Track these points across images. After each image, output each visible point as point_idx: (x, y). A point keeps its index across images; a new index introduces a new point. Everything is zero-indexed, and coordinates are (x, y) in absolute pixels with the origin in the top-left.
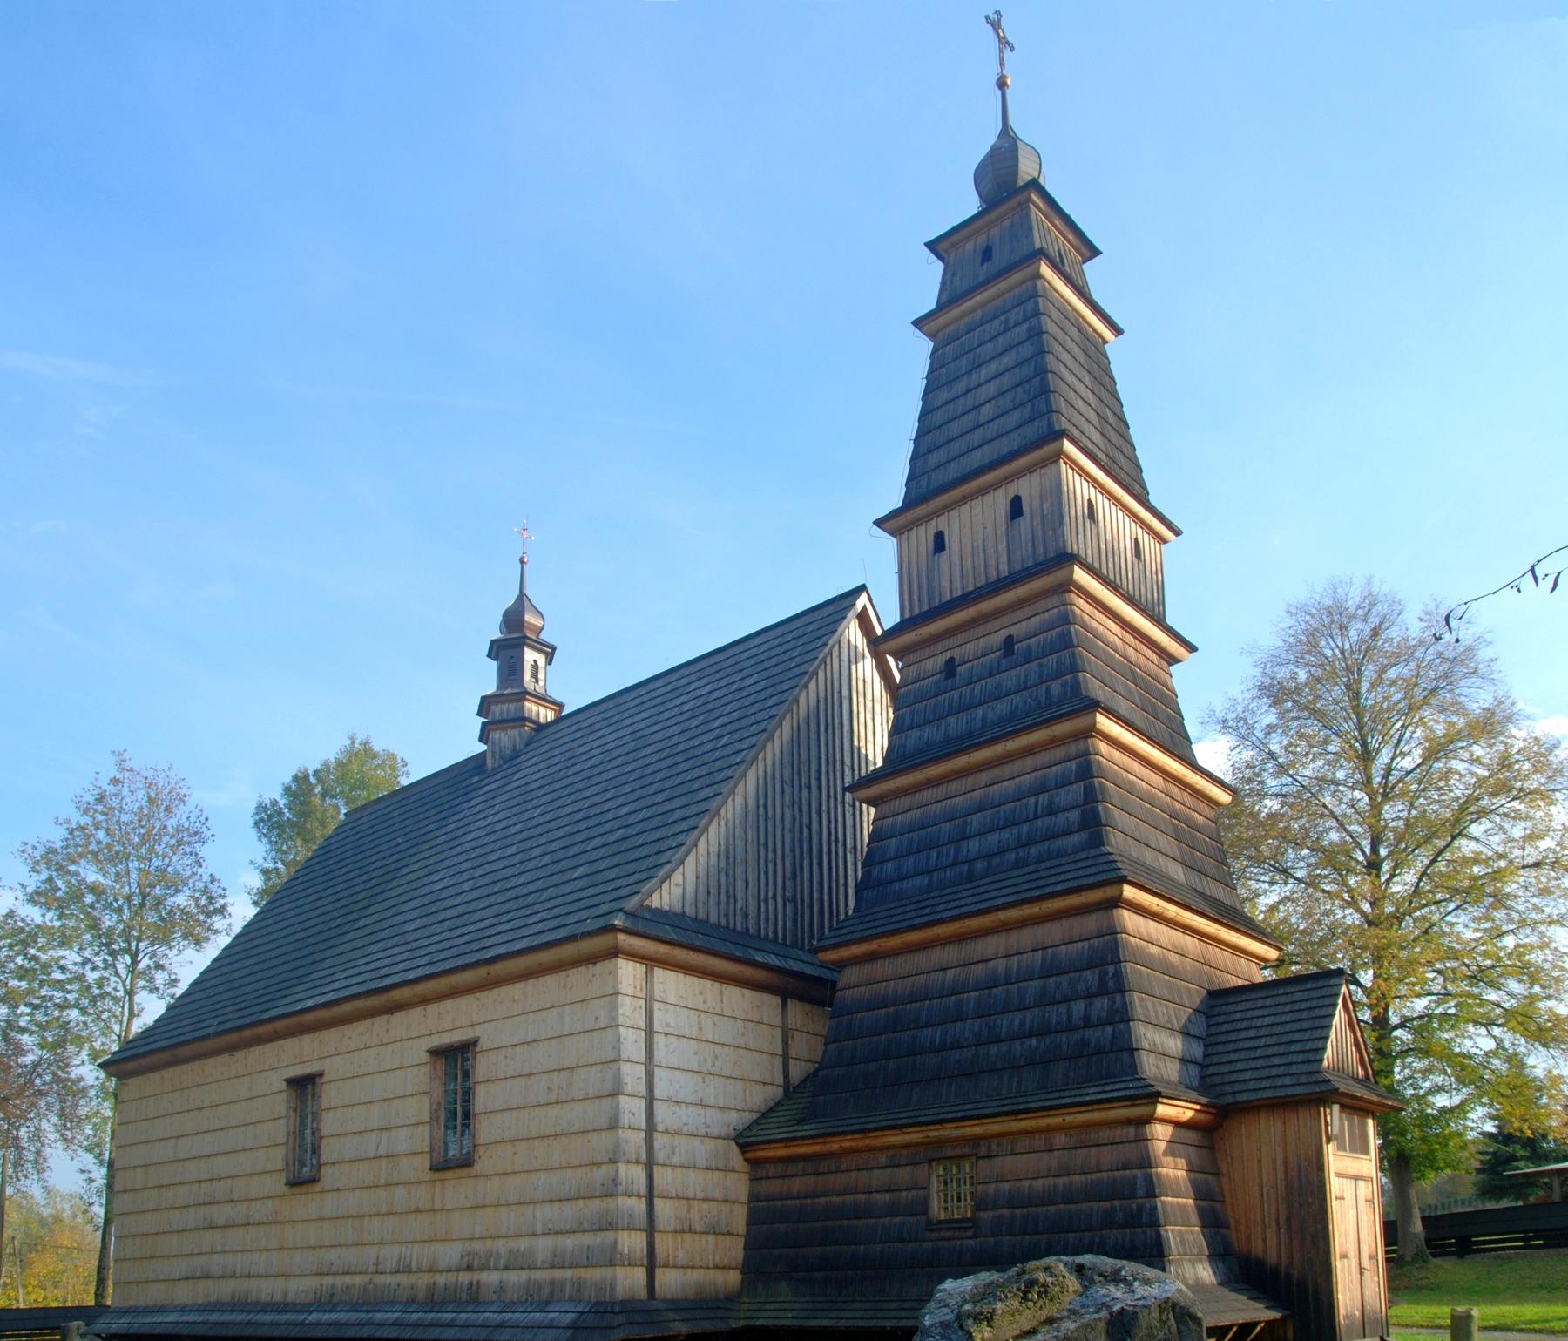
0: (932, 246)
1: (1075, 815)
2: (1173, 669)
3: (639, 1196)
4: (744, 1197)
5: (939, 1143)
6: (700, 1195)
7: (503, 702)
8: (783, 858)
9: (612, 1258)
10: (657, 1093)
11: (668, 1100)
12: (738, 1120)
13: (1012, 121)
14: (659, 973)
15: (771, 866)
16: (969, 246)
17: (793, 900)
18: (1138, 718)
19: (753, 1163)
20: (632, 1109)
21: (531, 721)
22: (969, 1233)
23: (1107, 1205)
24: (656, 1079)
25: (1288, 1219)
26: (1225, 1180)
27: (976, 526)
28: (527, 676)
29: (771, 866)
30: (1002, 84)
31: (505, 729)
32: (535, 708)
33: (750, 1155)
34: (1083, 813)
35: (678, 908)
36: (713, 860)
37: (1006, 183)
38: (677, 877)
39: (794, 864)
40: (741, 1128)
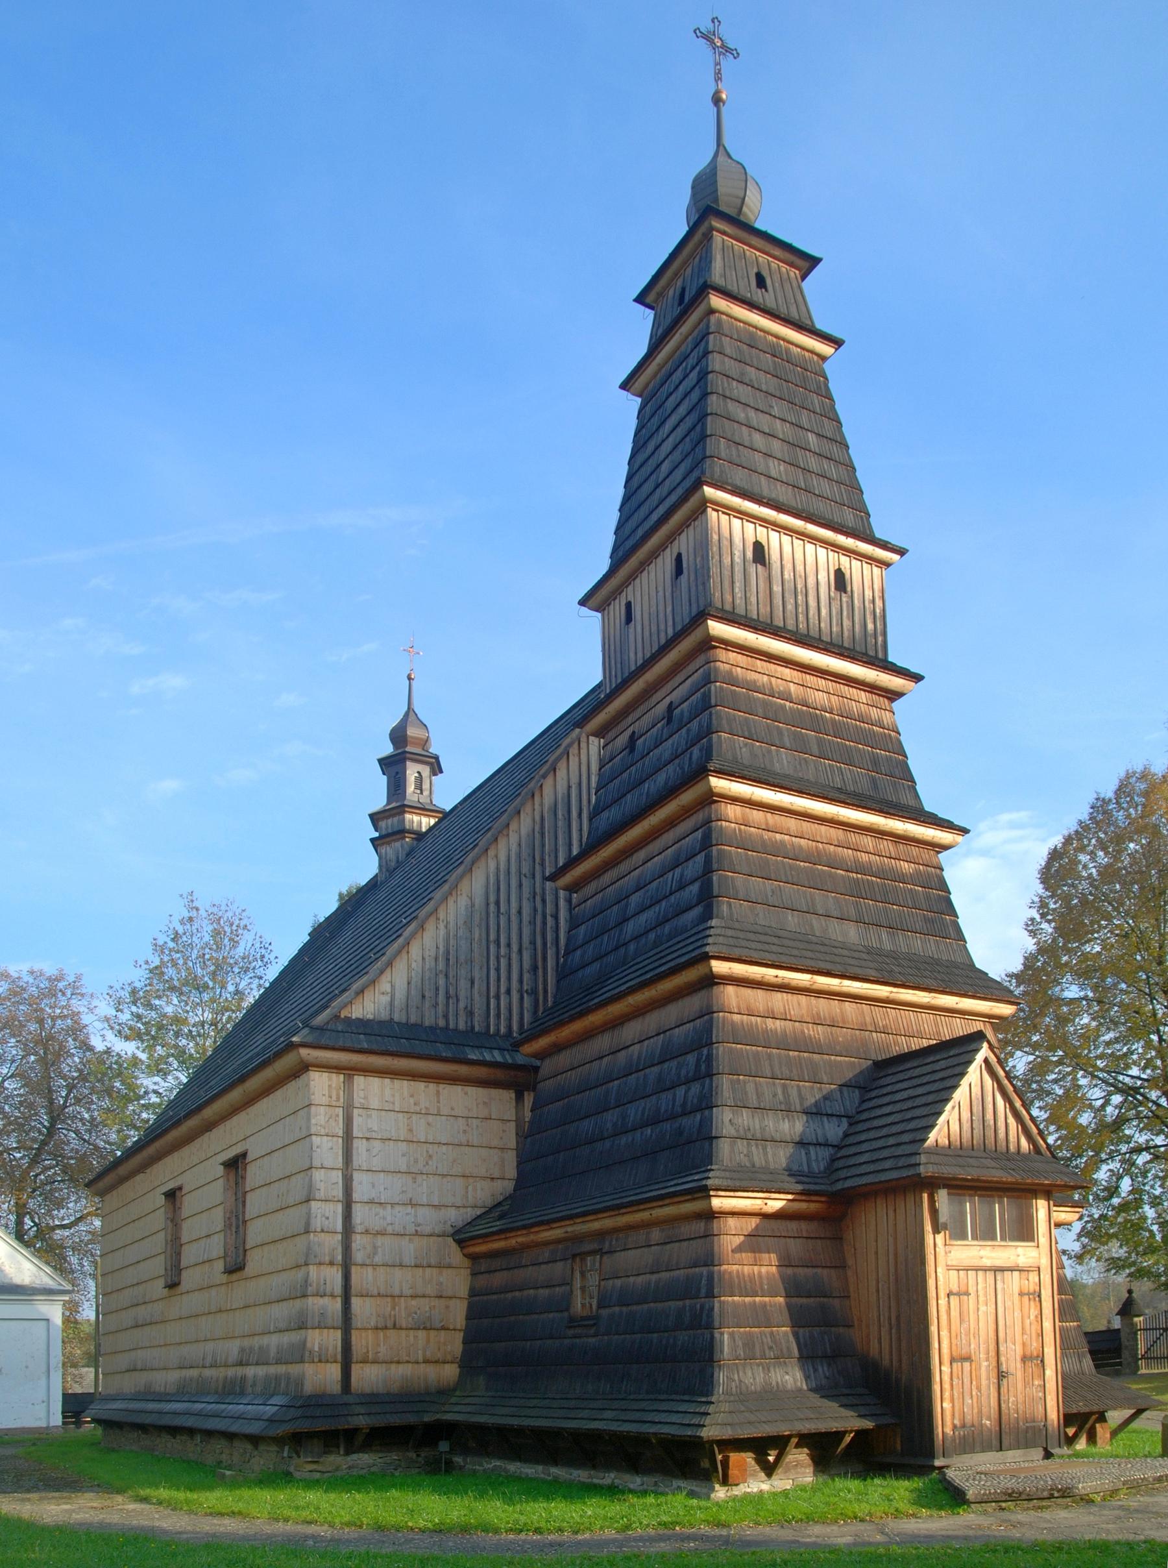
0: (640, 299)
2: (896, 705)
3: (333, 1296)
4: (464, 1291)
5: (578, 1239)
6: (408, 1292)
7: (388, 818)
8: (520, 951)
9: (299, 1354)
10: (356, 1196)
11: (371, 1202)
12: (456, 1217)
13: (727, 142)
14: (359, 1081)
15: (503, 962)
16: (671, 292)
17: (534, 992)
19: (474, 1258)
20: (328, 1214)
21: (410, 832)
22: (592, 1331)
23: (681, 1303)
24: (355, 1183)
26: (849, 1273)
27: (651, 589)
28: (411, 788)
29: (503, 962)
30: (717, 100)
31: (389, 843)
32: (416, 818)
33: (466, 1251)
34: (701, 888)
35: (384, 1015)
36: (429, 963)
38: (384, 985)
39: (534, 957)
40: (460, 1224)
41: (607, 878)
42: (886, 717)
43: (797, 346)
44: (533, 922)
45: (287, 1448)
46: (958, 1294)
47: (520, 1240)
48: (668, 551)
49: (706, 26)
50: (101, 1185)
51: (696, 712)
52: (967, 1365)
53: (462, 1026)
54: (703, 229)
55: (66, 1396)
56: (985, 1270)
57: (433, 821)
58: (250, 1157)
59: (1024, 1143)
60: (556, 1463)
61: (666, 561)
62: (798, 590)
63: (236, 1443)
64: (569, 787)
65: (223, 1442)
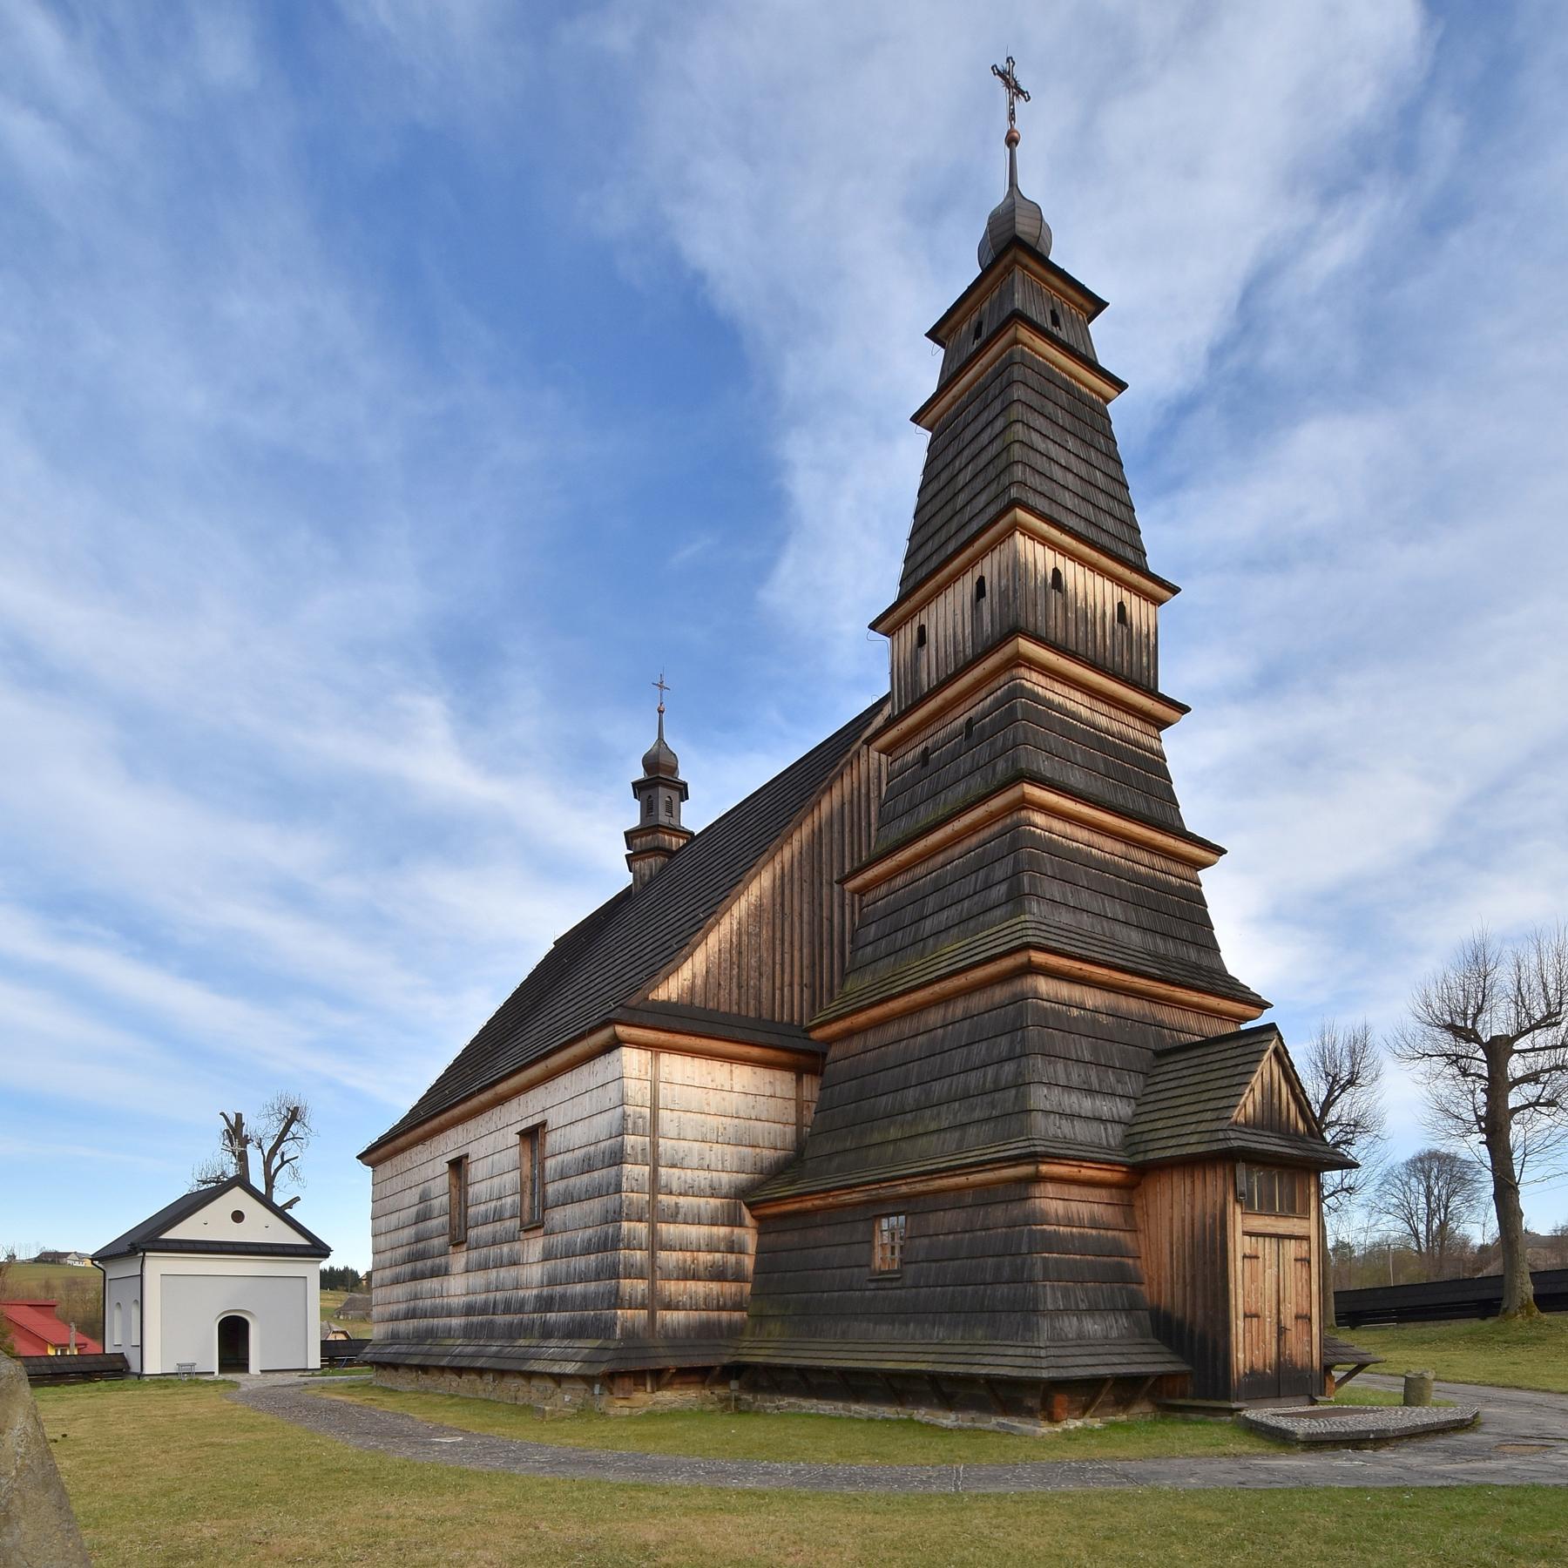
0: (933, 334)
1: (1003, 888)
9: (616, 1300)
14: (665, 1058)
16: (965, 327)
18: (1096, 786)
25: (1193, 1277)
26: (1141, 1237)
27: (949, 614)
30: (1012, 141)
34: (1010, 889)
35: (687, 999)
37: (1014, 246)
41: (899, 881)
42: (1155, 743)
43: (1086, 386)
44: (811, 923)
45: (597, 1387)
46: (1250, 1257)
47: (817, 1202)
48: (969, 575)
49: (1002, 65)
50: (374, 1156)
51: (998, 726)
52: (1255, 1320)
53: (752, 1014)
54: (1006, 261)
55: (325, 1345)
56: (1271, 1236)
57: (682, 842)
58: (550, 1126)
59: (1301, 1125)
60: (857, 1401)
61: (967, 585)
62: (1085, 618)
63: (535, 1382)
64: (843, 804)
65: (520, 1381)
